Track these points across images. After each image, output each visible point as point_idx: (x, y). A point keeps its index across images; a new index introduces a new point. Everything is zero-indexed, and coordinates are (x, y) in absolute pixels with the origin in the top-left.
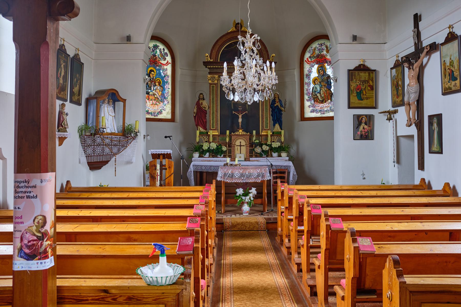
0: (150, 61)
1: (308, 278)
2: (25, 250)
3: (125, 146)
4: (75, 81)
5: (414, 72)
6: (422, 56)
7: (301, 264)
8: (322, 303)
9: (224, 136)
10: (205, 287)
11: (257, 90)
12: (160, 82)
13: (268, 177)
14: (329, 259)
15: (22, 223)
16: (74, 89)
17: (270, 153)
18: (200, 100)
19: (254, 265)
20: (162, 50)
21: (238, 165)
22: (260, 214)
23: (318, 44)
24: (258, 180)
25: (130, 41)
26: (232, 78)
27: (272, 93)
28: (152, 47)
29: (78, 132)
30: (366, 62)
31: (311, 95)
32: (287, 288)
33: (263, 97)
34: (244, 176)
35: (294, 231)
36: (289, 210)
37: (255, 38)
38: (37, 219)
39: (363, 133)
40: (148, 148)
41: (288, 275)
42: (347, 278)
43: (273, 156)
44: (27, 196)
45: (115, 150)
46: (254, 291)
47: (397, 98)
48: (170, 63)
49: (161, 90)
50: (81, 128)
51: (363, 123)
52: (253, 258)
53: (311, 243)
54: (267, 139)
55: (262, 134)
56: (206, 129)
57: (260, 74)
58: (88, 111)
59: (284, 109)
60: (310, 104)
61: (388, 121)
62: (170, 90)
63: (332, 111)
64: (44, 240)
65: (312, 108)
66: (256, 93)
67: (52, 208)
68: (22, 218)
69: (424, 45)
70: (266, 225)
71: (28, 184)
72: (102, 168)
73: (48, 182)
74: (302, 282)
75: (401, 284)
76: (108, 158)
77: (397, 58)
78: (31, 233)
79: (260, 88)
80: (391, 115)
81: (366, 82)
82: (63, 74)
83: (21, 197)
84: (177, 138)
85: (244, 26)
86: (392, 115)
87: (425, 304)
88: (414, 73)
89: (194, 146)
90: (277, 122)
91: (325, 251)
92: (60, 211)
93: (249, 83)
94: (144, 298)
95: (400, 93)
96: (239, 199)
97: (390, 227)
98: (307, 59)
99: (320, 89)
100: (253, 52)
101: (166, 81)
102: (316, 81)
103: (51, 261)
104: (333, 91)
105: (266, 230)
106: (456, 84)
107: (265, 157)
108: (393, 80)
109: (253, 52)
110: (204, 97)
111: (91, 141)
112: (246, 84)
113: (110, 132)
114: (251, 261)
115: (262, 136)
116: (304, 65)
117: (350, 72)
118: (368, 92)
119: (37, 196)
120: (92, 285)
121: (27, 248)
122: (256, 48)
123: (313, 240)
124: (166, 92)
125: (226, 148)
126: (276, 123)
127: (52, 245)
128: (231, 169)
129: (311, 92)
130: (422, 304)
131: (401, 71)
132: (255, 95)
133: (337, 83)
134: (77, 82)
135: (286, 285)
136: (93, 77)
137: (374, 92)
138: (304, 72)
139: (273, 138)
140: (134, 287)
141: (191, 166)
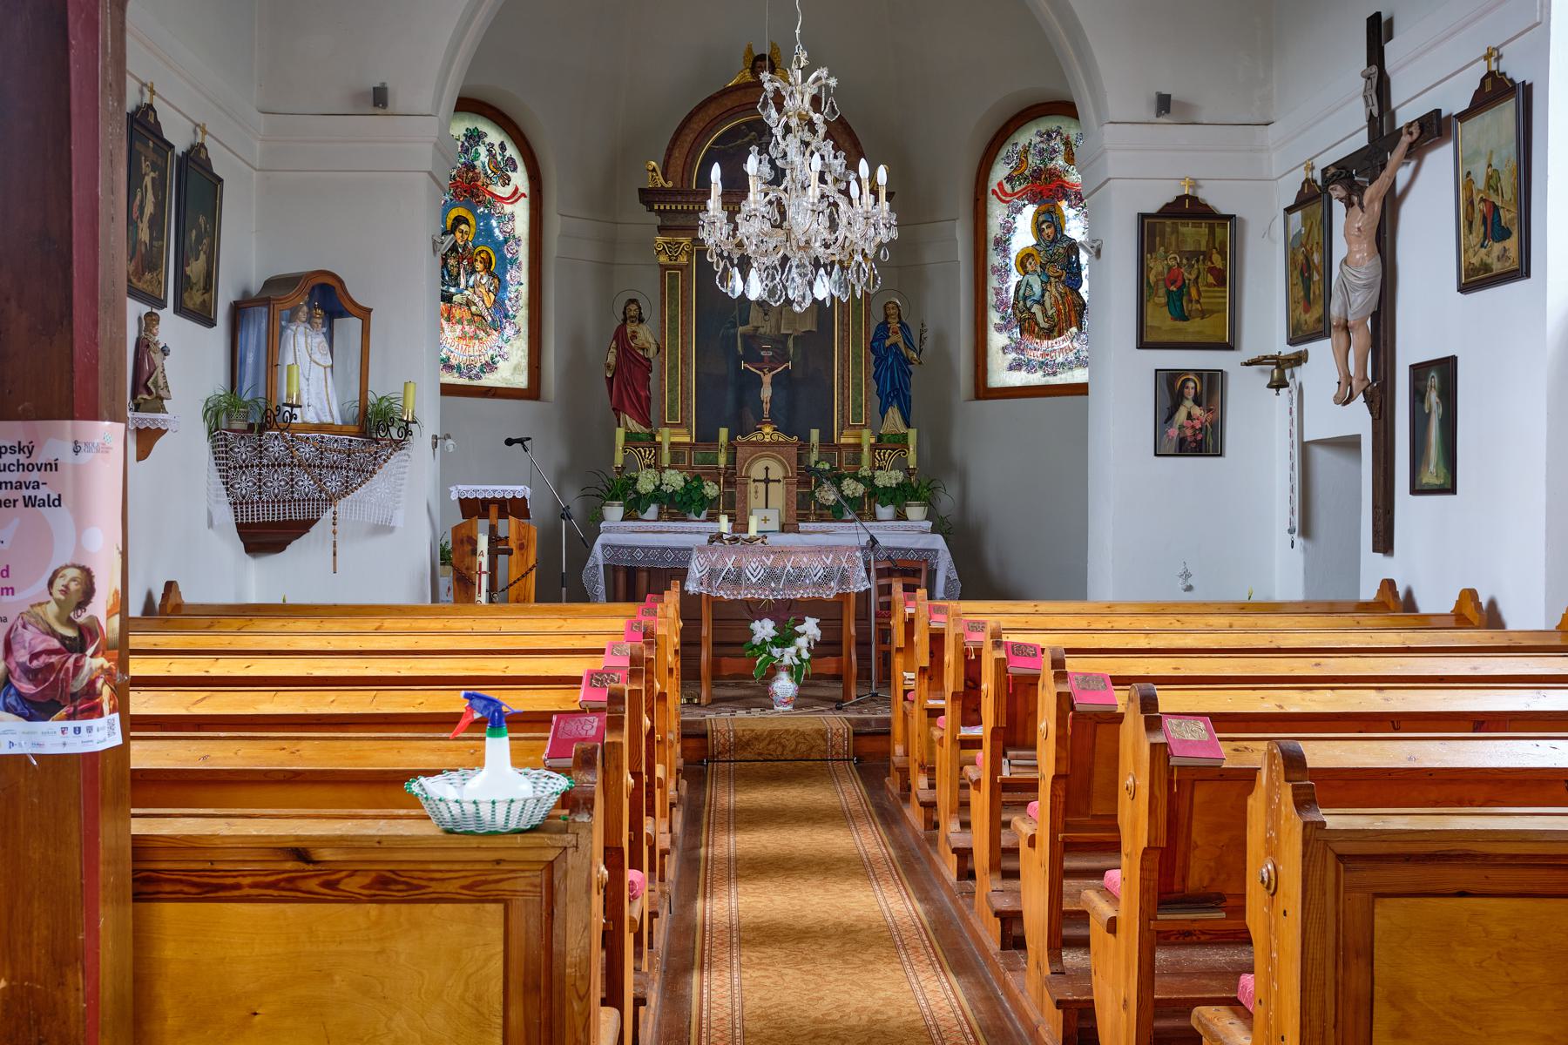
0: (455, 186)
1: (995, 888)
2: (21, 684)
3: (366, 473)
4: (193, 238)
5: (1366, 216)
6: (1393, 158)
7: (972, 853)
8: (1041, 959)
9: (709, 449)
10: (642, 889)
11: (826, 262)
12: (490, 258)
13: (860, 582)
14: (1066, 811)
15: (10, 591)
16: (188, 265)
17: (870, 508)
18: (628, 321)
19: (812, 861)
20: (497, 149)
21: (759, 541)
22: (831, 709)
23: (1037, 134)
24: (828, 593)
25: (385, 105)
26: (739, 218)
27: (876, 272)
28: (463, 139)
29: (205, 417)
30: (1200, 187)
31: (1010, 310)
32: (921, 930)
33: (847, 287)
34: (777, 579)
35: (947, 742)
36: (930, 679)
37: (819, 83)
38: (61, 577)
39: (1189, 432)
40: (447, 478)
41: (928, 892)
42: (1127, 855)
43: (880, 517)
44: (24, 497)
45: (333, 483)
46: (809, 938)
47: (1307, 310)
48: (523, 195)
49: (491, 288)
50: (215, 406)
51: (1187, 399)
52: (807, 840)
53: (1006, 773)
54: (857, 461)
55: (843, 441)
56: (648, 424)
57: (835, 205)
58: (239, 349)
59: (918, 355)
60: (1007, 342)
61: (1275, 390)
62: (524, 289)
63: (1081, 363)
64: (86, 650)
65: (1013, 355)
66: (822, 271)
67: (115, 547)
68: (8, 576)
69: (1401, 120)
70: (851, 742)
71: (28, 457)
72: (289, 547)
73: (99, 454)
74: (973, 908)
75: (1308, 830)
76: (308, 512)
77: (1307, 174)
78: (40, 627)
79: (835, 253)
80: (1283, 370)
81: (1201, 257)
82: (149, 209)
83: (5, 503)
84: (549, 453)
85: (781, 66)
86: (1288, 372)
87: (1387, 900)
88: (1365, 219)
89: (605, 480)
90: (892, 400)
91: (1052, 782)
92: (143, 662)
93: (798, 233)
94: (432, 879)
95: (1314, 293)
96: (761, 655)
97: (1273, 703)
98: (1000, 185)
99: (1044, 290)
100: (813, 131)
101: (509, 256)
102: (1030, 260)
103: (111, 727)
104: (1086, 297)
105: (853, 760)
106: (1505, 250)
107: (851, 521)
108: (1294, 249)
109: (811, 125)
110: (641, 313)
111: (249, 449)
112: (787, 241)
113: (317, 422)
114: (801, 848)
115: (839, 447)
116: (989, 206)
117: (1146, 221)
118: (1206, 291)
119: (59, 500)
120: (255, 833)
121: (28, 678)
122: (821, 117)
123: (1012, 762)
124: (509, 295)
125: (716, 487)
126: (891, 405)
127: (115, 676)
128: (735, 553)
129: (1012, 300)
130: (1378, 901)
131: (1319, 217)
132: (818, 278)
133: (1100, 260)
134: (201, 243)
135: (920, 919)
136: (256, 231)
137: (1226, 292)
138: (989, 231)
139: (880, 456)
140: (398, 839)
141: (595, 547)
